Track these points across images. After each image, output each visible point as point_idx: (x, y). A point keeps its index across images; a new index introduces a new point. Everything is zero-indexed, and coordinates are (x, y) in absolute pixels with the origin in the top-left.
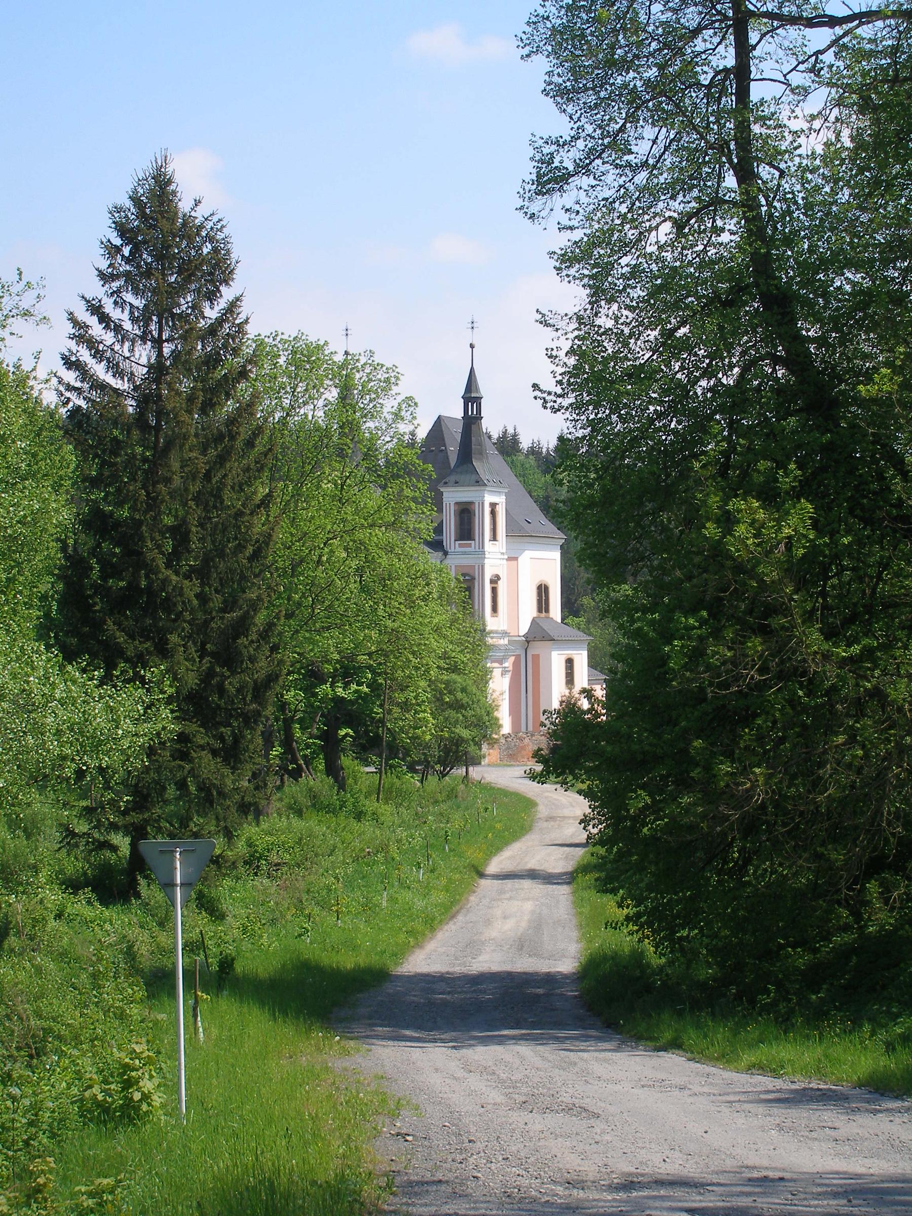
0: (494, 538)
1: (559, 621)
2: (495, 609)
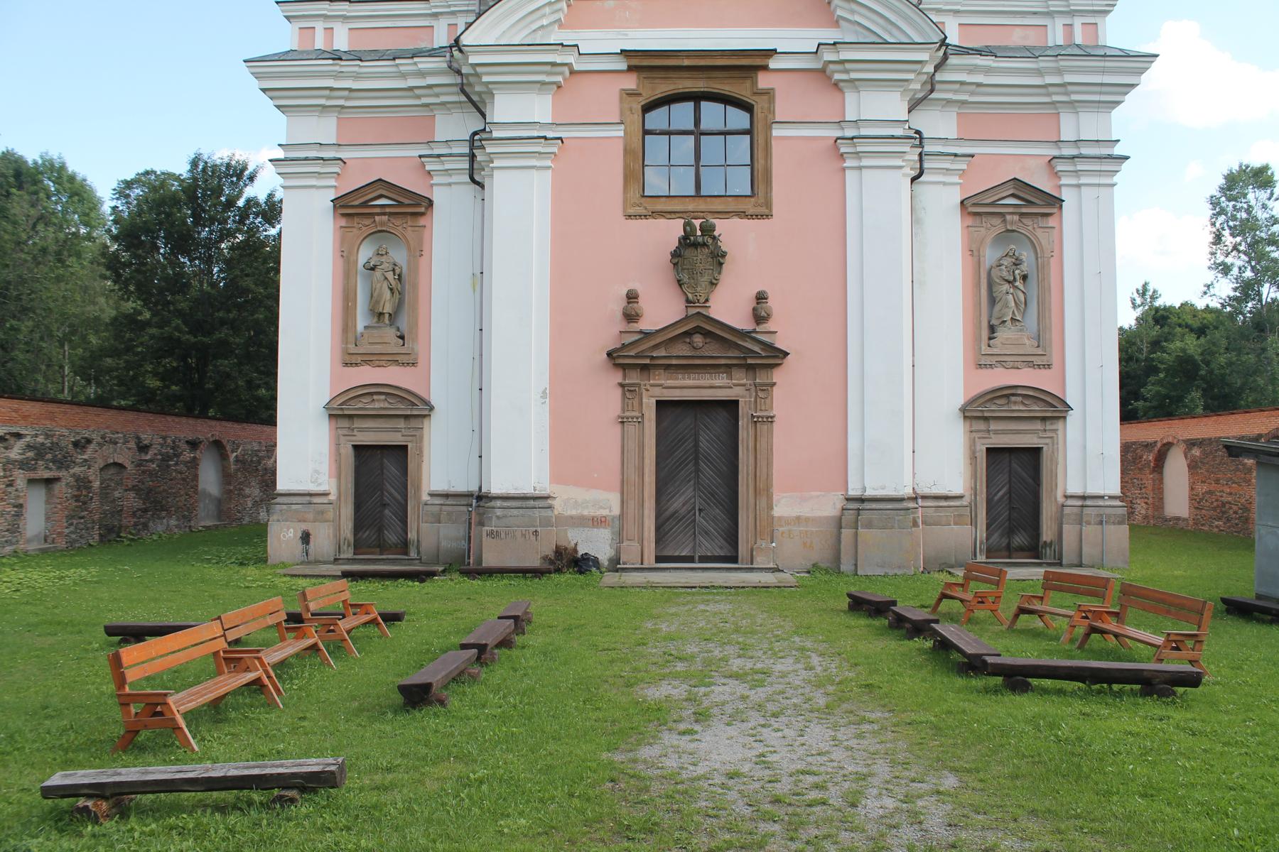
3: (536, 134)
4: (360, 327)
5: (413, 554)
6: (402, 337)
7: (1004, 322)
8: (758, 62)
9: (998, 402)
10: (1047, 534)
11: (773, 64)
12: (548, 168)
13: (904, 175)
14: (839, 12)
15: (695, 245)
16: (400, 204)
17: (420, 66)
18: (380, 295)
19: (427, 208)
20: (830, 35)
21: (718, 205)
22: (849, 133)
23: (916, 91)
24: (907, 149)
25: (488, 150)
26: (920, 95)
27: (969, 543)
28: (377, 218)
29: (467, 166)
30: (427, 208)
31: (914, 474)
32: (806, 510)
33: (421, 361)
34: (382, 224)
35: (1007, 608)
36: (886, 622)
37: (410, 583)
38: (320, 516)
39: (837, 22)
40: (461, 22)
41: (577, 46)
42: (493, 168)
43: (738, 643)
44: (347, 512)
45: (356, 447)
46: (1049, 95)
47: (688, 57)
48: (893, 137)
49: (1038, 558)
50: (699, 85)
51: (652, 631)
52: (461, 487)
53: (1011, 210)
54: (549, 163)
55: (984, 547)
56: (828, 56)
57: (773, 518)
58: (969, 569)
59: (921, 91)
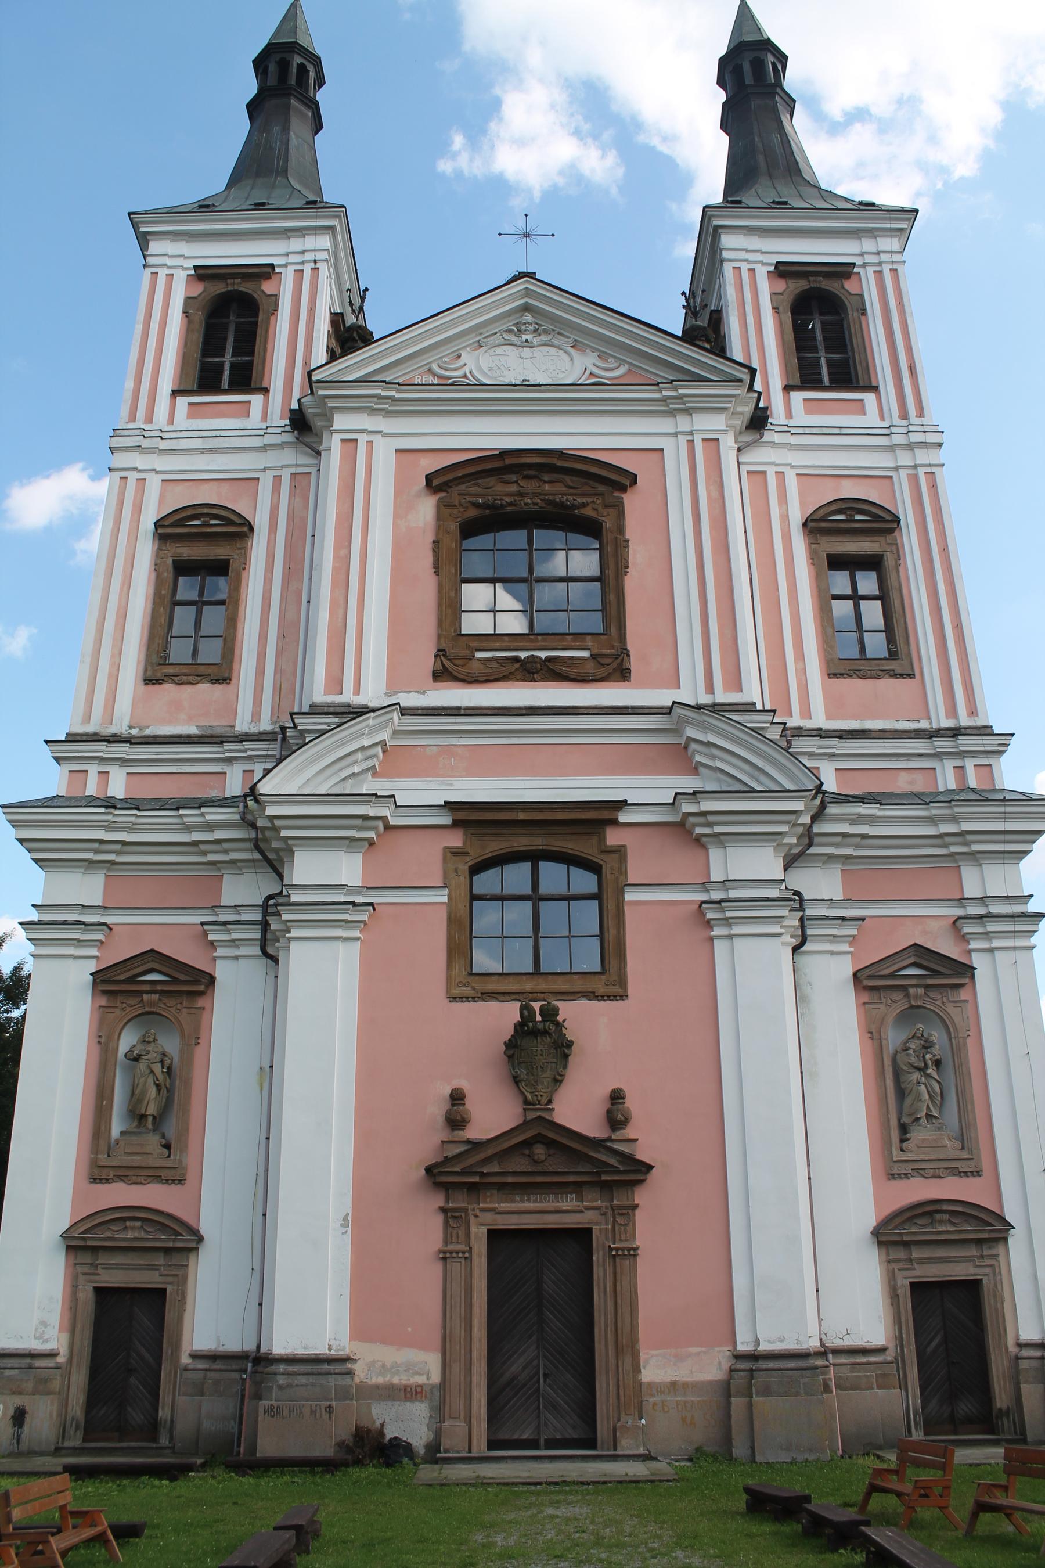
3: (342, 899)
4: (115, 1131)
5: (164, 1441)
6: (167, 1146)
7: (918, 1119)
8: (605, 815)
9: (919, 1221)
10: (1001, 1399)
11: (623, 818)
12: (357, 939)
13: (784, 944)
14: (698, 758)
15: (535, 1033)
16: (175, 980)
17: (208, 817)
18: (144, 1092)
19: (207, 986)
20: (688, 783)
21: (562, 985)
22: (716, 895)
23: (791, 846)
24: (786, 913)
25: (285, 917)
26: (796, 850)
27: (900, 1413)
28: (145, 997)
29: (258, 936)
30: (207, 986)
31: (820, 1321)
32: (683, 1373)
33: (190, 1177)
34: (152, 1004)
35: (961, 1505)
36: (799, 1528)
37: (157, 1482)
38: (42, 1386)
39: (696, 769)
40: (258, 768)
41: (393, 796)
42: (290, 939)
43: (601, 1561)
44: (79, 1379)
45: (97, 1290)
46: (946, 846)
47: (523, 810)
48: (768, 899)
49: (993, 1433)
50: (536, 842)
51: (484, 1546)
52: (233, 1345)
53: (914, 982)
54: (357, 933)
55: (920, 1419)
56: (687, 807)
57: (640, 1384)
58: (903, 1448)
59: (797, 845)
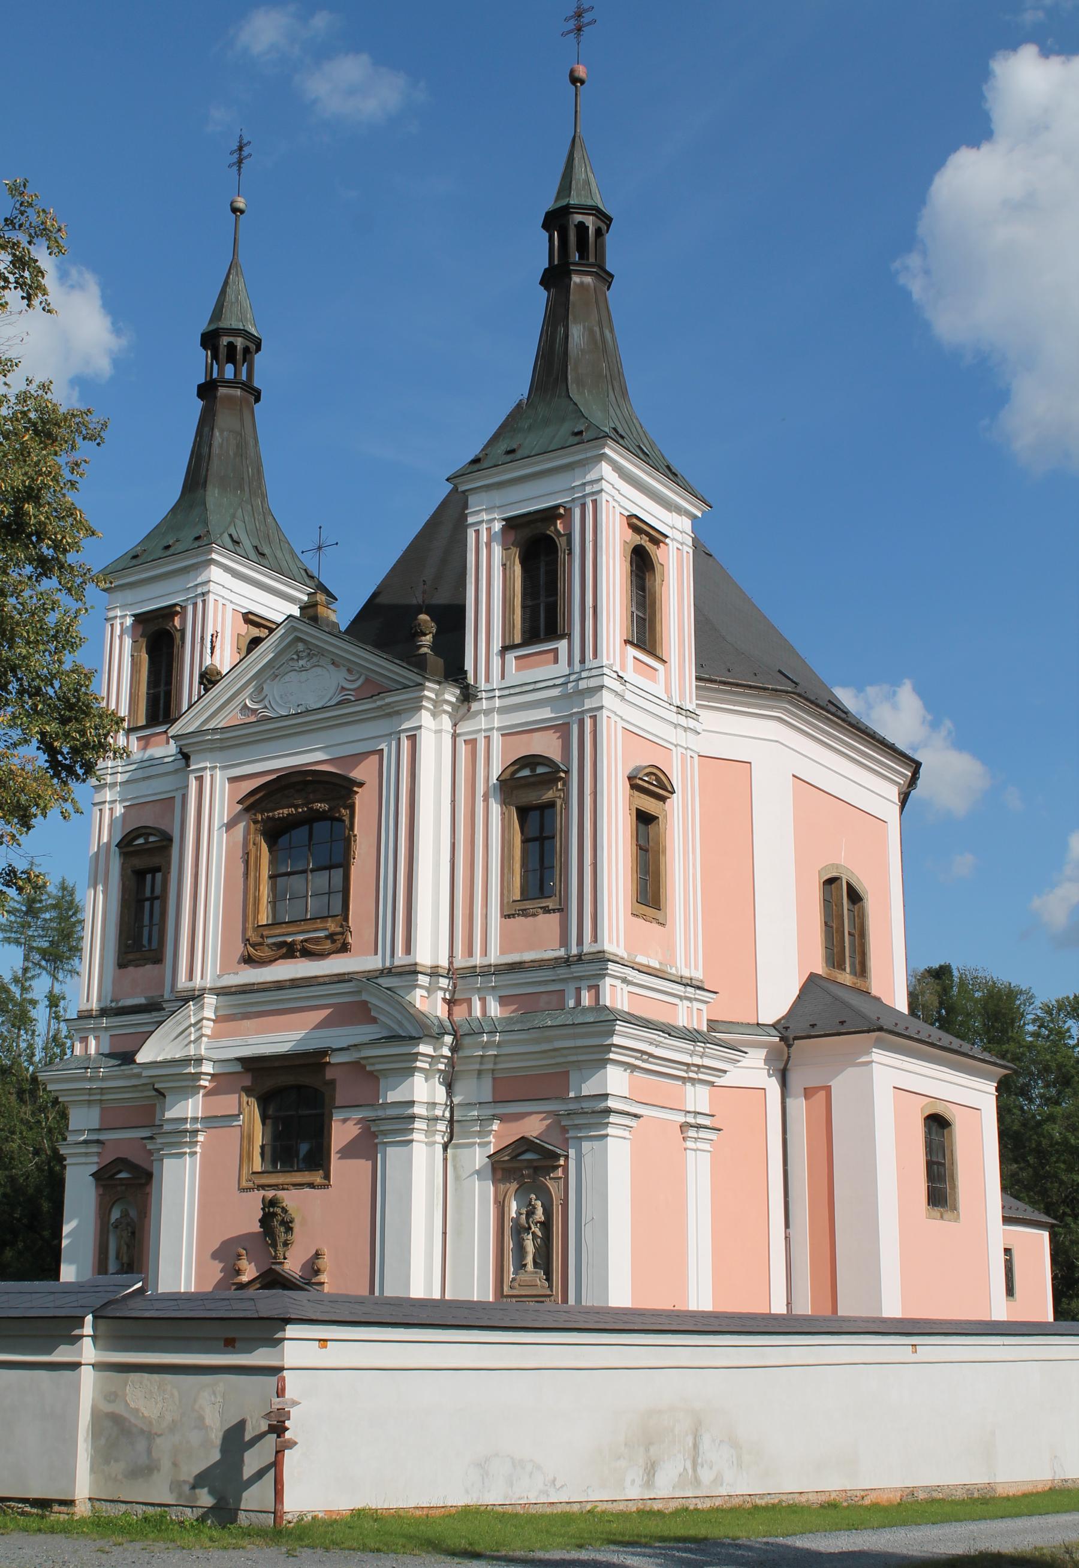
0: (645, 635)
1: (901, 1005)
2: (649, 892)
28: (119, 1188)
